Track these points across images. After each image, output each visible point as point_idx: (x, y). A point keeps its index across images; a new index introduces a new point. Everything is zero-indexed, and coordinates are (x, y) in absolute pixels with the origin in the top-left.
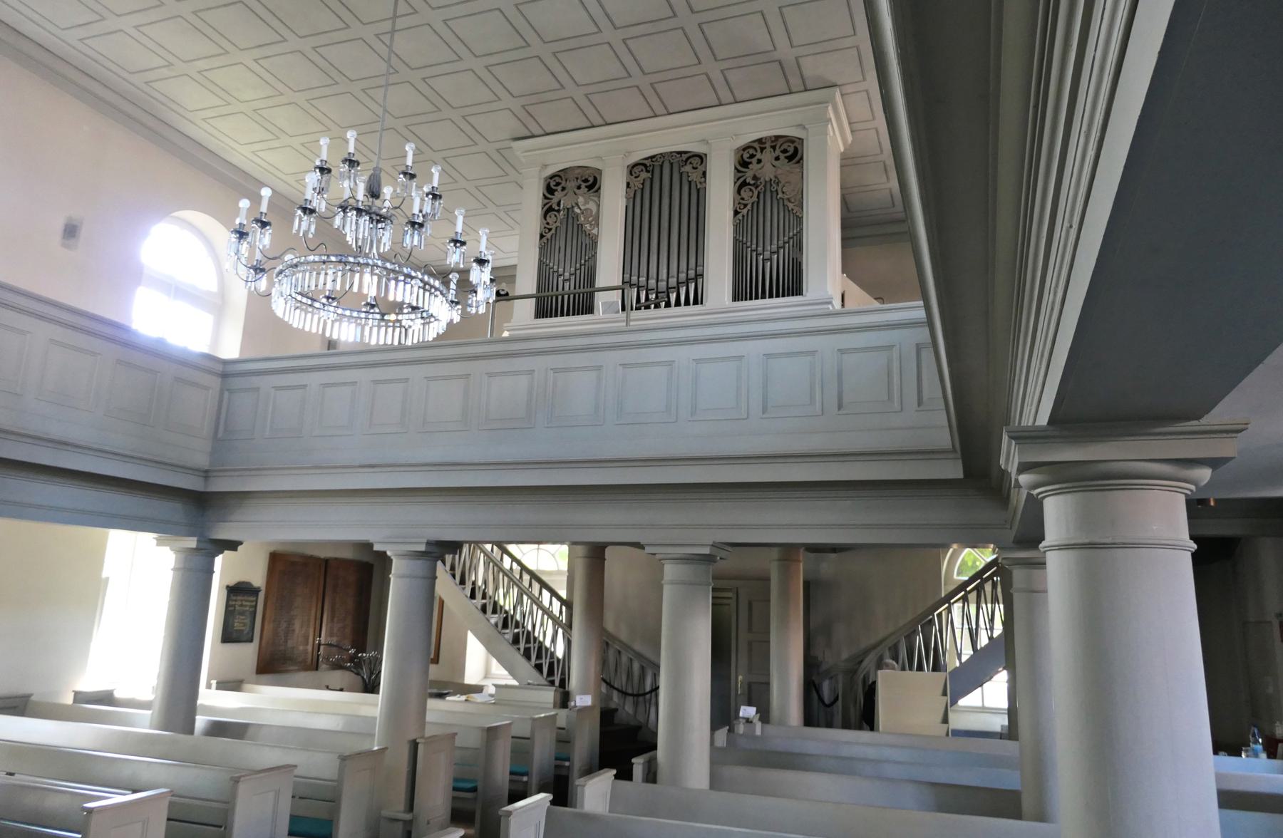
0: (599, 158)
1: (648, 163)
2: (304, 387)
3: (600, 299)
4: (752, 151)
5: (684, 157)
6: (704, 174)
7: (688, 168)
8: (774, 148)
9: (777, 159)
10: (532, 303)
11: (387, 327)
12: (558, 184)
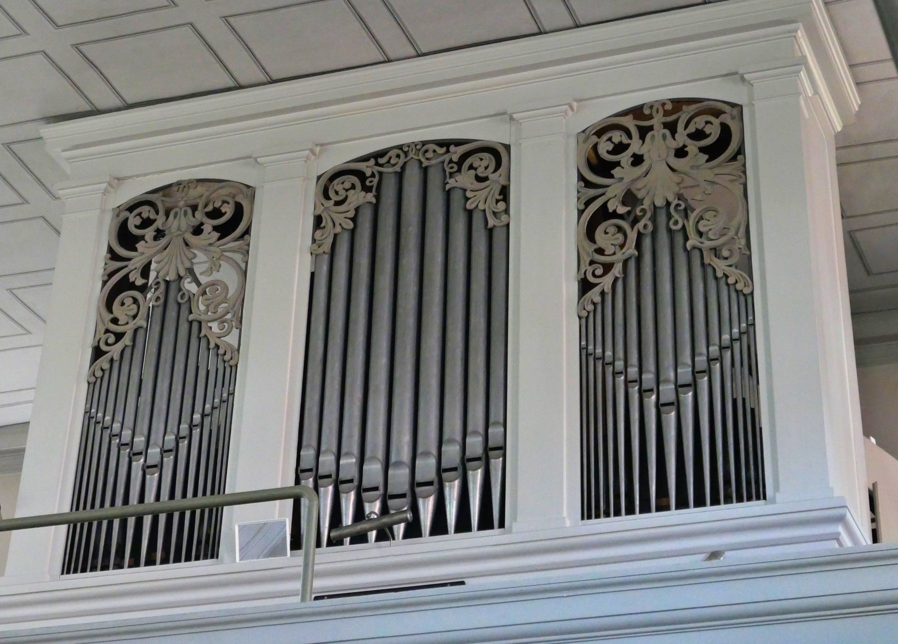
0: (250, 159)
1: (367, 168)
3: (236, 521)
4: (618, 137)
5: (456, 152)
6: (505, 192)
7: (465, 179)
8: (672, 127)
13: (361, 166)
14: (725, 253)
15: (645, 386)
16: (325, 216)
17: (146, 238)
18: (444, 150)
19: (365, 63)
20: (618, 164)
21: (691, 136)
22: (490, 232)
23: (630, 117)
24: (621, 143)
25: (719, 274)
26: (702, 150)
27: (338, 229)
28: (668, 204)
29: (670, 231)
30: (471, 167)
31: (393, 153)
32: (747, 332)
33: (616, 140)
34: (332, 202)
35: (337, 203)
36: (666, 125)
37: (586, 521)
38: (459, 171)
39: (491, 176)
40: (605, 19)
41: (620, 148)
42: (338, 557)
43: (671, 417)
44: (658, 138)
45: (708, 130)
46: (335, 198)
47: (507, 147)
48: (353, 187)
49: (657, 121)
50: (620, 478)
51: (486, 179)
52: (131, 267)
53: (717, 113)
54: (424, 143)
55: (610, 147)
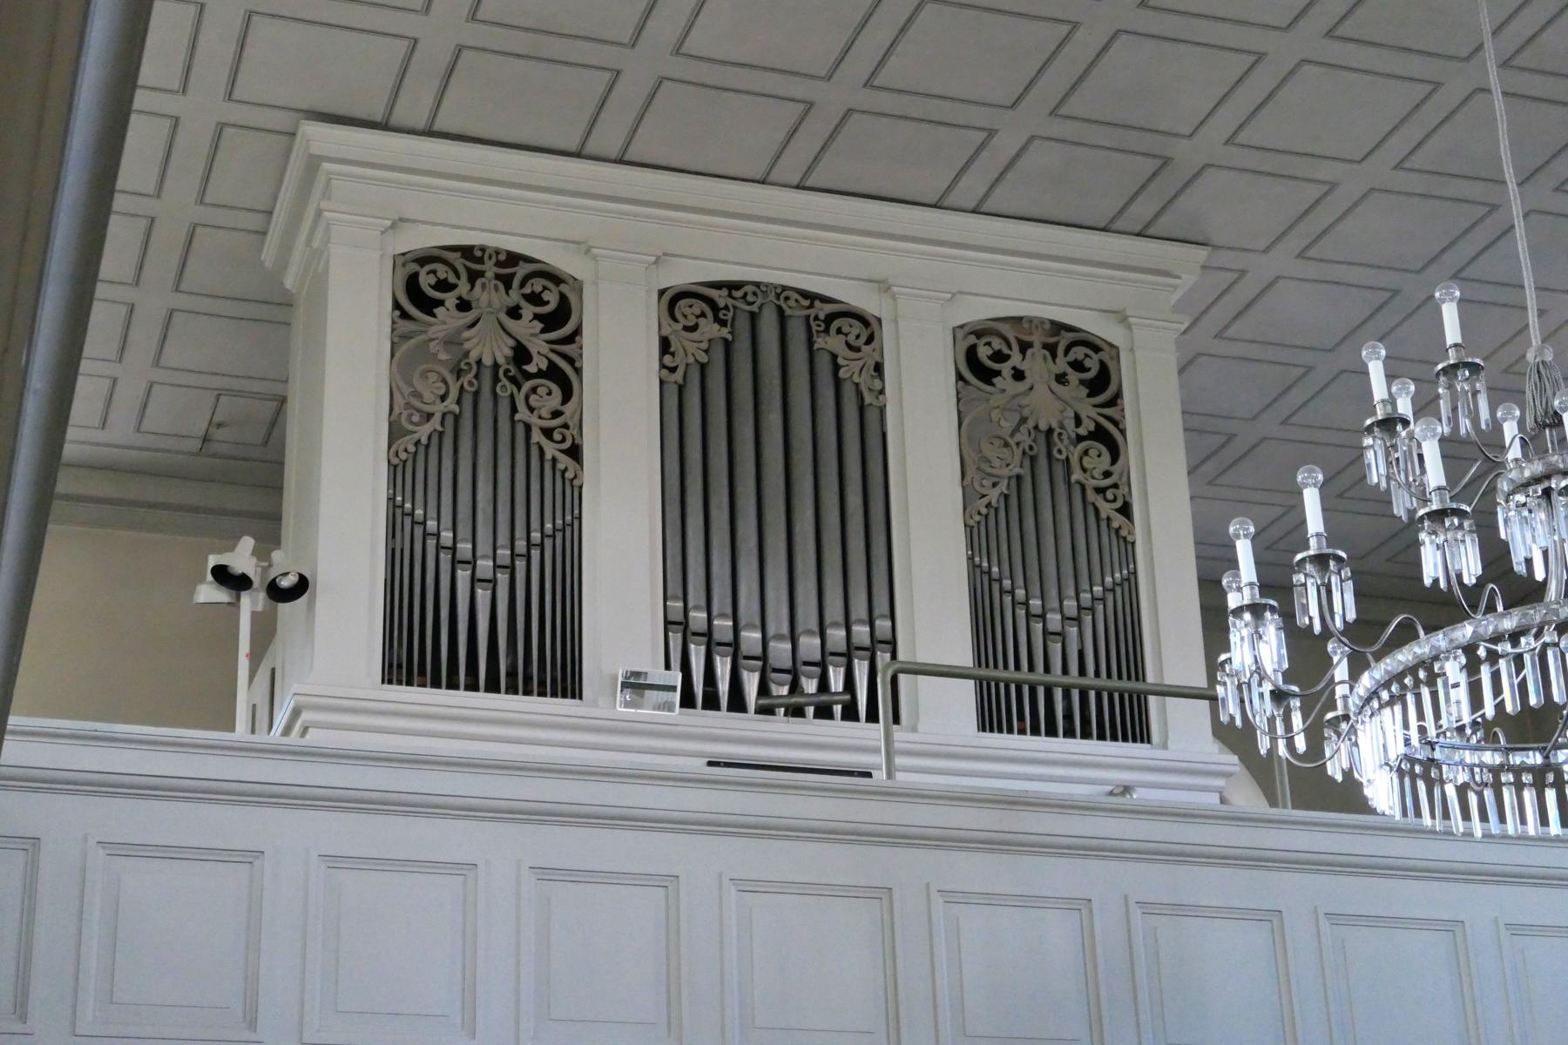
0: (586, 249)
1: (720, 297)
2: (251, 856)
3: (918, 692)
4: (443, 272)
5: (823, 310)
6: (879, 368)
7: (833, 343)
8: (1051, 349)
9: (1061, 379)
10: (965, 691)
11: (1519, 786)
12: (444, 286)
13: (714, 293)
14: (557, 436)
15: (459, 556)
16: (672, 339)
17: (447, 304)
18: (806, 303)
19: (883, 193)
20: (998, 373)
21: (525, 297)
22: (862, 409)
23: (458, 254)
24: (1000, 351)
25: (1103, 515)
26: (1082, 382)
27: (691, 360)
28: (496, 366)
29: (495, 395)
30: (839, 331)
31: (749, 289)
32: (1128, 580)
33: (442, 276)
34: (679, 327)
35: (686, 329)
36: (1046, 346)
37: (386, 686)
38: (827, 331)
39: (864, 348)
40: (890, 195)
41: (999, 357)
42: (739, 724)
43: (483, 595)
44: (1040, 359)
45: (1088, 363)
46: (683, 322)
47: (662, 293)
48: (703, 315)
49: (1037, 339)
50: (420, 651)
51: (858, 350)
52: (431, 334)
53: (1097, 349)
54: (785, 288)
55: (990, 352)
